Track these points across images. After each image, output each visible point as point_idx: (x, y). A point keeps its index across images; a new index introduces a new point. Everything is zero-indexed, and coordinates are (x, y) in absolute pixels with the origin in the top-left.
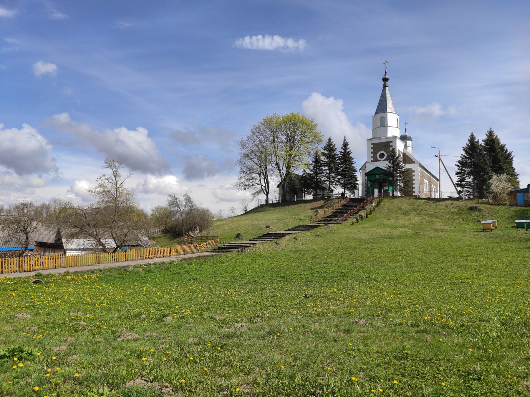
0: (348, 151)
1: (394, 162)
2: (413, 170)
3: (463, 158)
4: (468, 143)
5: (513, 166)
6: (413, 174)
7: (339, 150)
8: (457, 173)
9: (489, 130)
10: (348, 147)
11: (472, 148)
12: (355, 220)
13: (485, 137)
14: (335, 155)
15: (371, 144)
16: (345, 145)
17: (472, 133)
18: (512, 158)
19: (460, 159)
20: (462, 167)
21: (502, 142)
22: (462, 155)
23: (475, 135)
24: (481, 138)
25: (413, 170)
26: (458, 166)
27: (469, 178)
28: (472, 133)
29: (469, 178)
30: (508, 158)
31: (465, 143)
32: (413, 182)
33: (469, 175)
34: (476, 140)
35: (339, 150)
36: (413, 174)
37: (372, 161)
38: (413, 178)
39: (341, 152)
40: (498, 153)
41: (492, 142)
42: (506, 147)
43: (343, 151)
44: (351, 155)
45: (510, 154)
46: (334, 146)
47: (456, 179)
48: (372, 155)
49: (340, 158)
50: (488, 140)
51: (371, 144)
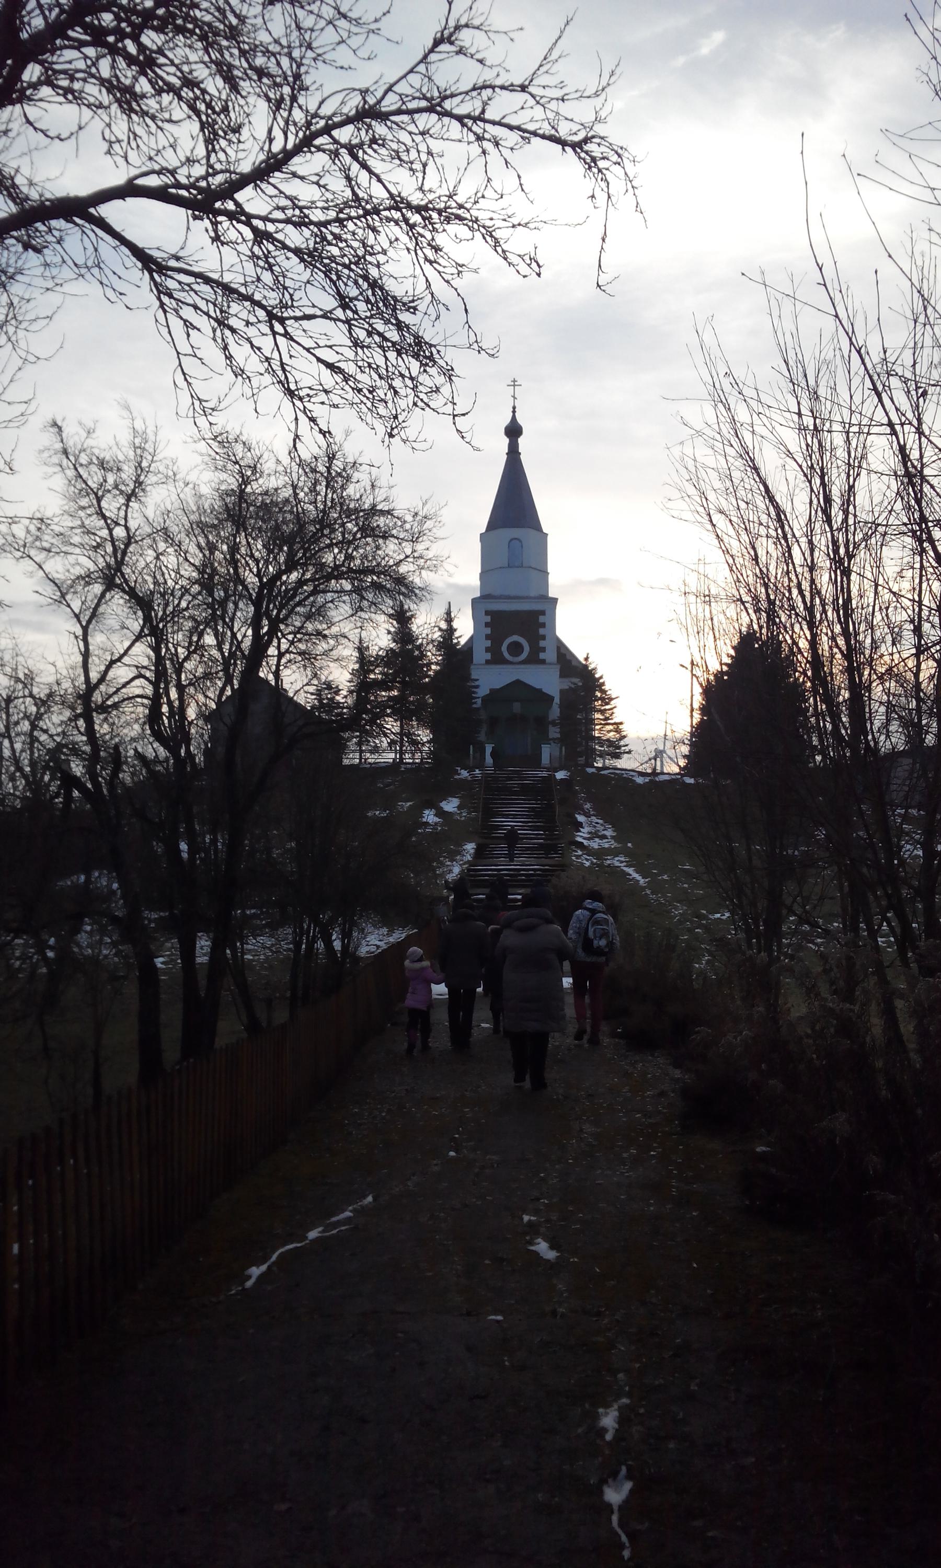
16: (514, 507)
37: (488, 662)
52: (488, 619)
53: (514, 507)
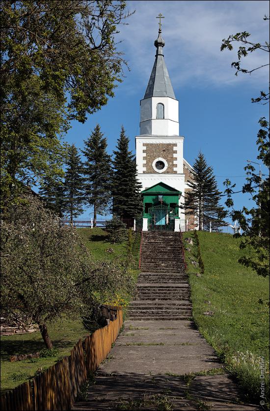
15: (144, 145)
37: (144, 173)
51: (144, 145)
52: (145, 148)
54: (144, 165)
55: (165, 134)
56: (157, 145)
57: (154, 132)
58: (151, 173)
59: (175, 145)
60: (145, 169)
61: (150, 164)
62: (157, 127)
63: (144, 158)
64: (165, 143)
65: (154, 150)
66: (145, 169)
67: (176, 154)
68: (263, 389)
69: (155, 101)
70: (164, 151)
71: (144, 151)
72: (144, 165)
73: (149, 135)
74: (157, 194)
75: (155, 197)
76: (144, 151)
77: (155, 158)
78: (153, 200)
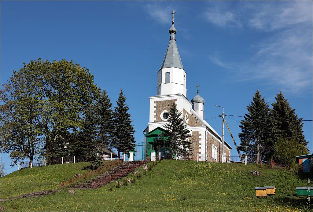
0: (124, 107)
1: (174, 120)
2: (200, 133)
3: (246, 119)
4: (253, 101)
5: (303, 134)
6: (200, 137)
7: (114, 106)
8: (240, 136)
9: (279, 94)
10: (124, 103)
11: (257, 106)
12: (121, 183)
13: (275, 101)
14: (110, 111)
15: (155, 102)
16: (121, 100)
17: (257, 91)
18: (302, 125)
19: (244, 119)
20: (246, 128)
21: (292, 106)
22: (246, 115)
23: (261, 93)
24: (270, 101)
25: (200, 133)
26: (241, 127)
27: (253, 141)
28: (257, 91)
29: (253, 141)
30: (298, 124)
31: (250, 101)
32: (200, 146)
33: (253, 138)
34: (261, 99)
35: (114, 106)
36: (200, 137)
37: (155, 122)
38: (200, 142)
39: (117, 108)
40: (287, 118)
41: (281, 107)
42: (296, 113)
43: (118, 107)
44: (128, 112)
45: (300, 120)
46: (109, 100)
47: (239, 142)
48: (155, 114)
49: (116, 115)
50: (276, 104)
51: (155, 102)
52: (155, 105)
53: (121, 100)
54: (155, 117)
55: (170, 94)
56: (164, 102)
57: (163, 93)
58: (159, 121)
59: (176, 100)
60: (155, 119)
61: (159, 115)
62: (165, 89)
63: (155, 112)
64: (158, 101)
65: (162, 105)
66: (155, 119)
67: (155, 110)
68: (309, 199)
69: (164, 71)
70: (168, 105)
71: (155, 107)
72: (155, 117)
73: (160, 95)
74: (156, 136)
75: (155, 138)
76: (155, 107)
77: (162, 111)
78: (154, 140)
